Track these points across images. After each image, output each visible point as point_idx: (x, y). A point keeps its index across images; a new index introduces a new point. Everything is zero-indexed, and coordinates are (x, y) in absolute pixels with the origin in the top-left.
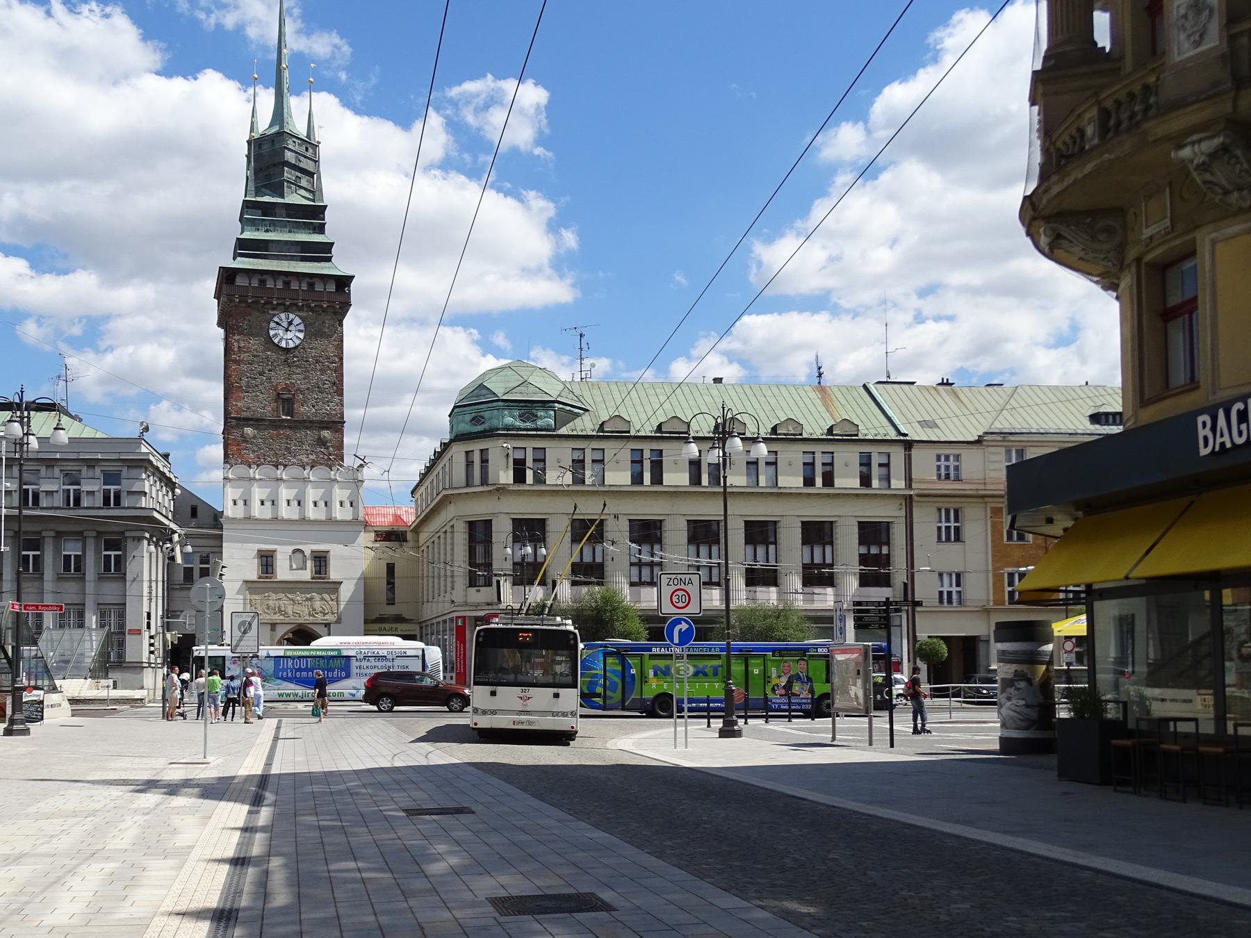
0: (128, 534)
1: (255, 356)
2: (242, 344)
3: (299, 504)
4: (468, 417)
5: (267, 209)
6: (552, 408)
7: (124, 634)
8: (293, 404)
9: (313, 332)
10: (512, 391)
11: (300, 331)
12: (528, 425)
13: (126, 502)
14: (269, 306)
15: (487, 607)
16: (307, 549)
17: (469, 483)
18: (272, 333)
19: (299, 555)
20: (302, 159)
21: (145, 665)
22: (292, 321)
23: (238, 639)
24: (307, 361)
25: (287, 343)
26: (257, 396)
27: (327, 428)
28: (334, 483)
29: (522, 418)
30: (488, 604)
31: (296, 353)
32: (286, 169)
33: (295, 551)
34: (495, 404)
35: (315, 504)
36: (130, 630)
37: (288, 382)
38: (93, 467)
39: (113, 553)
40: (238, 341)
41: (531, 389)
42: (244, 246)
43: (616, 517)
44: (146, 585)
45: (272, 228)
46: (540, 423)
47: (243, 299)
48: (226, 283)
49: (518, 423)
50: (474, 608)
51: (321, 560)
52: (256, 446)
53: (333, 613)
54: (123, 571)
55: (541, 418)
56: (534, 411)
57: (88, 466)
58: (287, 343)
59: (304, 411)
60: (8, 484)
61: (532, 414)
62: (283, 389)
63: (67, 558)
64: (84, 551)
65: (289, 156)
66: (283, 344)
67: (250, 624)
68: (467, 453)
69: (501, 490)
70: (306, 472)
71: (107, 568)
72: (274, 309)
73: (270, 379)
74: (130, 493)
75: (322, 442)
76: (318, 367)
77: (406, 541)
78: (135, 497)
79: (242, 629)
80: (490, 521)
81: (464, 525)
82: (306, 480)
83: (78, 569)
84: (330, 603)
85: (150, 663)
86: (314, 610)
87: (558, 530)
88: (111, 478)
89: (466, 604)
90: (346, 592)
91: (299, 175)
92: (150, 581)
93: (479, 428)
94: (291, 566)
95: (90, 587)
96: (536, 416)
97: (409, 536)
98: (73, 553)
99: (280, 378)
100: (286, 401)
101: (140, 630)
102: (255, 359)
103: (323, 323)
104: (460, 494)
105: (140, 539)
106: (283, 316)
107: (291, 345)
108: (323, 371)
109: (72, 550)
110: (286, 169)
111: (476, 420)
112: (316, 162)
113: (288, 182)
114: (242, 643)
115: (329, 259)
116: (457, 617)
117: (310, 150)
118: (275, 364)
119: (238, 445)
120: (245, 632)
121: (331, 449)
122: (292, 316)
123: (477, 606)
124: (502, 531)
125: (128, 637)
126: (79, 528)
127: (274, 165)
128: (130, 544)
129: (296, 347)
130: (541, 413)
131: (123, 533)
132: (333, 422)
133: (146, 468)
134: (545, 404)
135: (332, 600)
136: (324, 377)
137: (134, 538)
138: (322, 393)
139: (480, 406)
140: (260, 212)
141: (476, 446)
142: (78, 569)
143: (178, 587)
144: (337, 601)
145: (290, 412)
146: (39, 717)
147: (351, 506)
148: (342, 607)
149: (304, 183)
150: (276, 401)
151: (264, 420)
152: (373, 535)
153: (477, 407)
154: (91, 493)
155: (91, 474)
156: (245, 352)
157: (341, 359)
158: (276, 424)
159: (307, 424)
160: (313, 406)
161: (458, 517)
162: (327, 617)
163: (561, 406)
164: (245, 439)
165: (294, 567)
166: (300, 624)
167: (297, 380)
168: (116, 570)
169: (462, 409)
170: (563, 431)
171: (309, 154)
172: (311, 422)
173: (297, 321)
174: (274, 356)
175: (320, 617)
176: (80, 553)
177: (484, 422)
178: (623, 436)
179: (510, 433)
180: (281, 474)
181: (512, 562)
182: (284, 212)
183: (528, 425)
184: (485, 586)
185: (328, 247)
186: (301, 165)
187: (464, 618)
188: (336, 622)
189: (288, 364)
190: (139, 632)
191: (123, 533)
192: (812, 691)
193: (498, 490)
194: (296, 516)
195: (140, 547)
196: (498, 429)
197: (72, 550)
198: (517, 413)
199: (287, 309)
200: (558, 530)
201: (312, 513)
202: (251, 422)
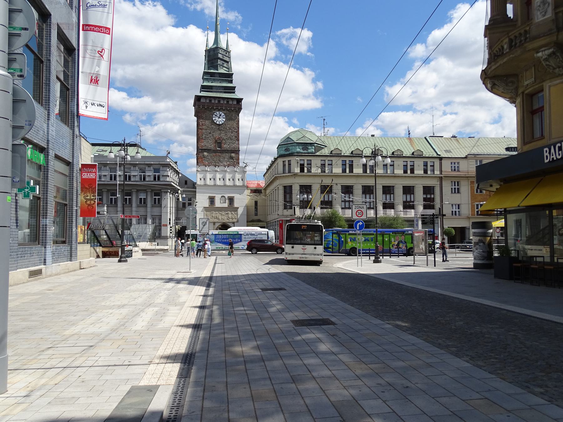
3: (223, 180)
4: (284, 149)
5: (212, 75)
7: (161, 226)
8: (221, 144)
9: (228, 119)
11: (224, 118)
12: (305, 151)
13: (161, 179)
18: (214, 119)
19: (223, 198)
20: (224, 57)
21: (168, 237)
25: (219, 122)
27: (233, 153)
29: (303, 149)
30: (291, 216)
33: (222, 197)
35: (229, 180)
37: (219, 136)
38: (150, 166)
39: (157, 197)
40: (202, 122)
41: (306, 139)
42: (204, 88)
43: (337, 184)
44: (169, 209)
45: (214, 81)
46: (309, 151)
49: (302, 151)
51: (231, 200)
53: (236, 219)
55: (310, 149)
58: (219, 122)
59: (225, 146)
60: (120, 173)
61: (307, 148)
62: (218, 139)
63: (141, 199)
65: (220, 56)
66: (218, 123)
67: (206, 223)
68: (283, 161)
69: (295, 175)
71: (155, 203)
72: (214, 110)
74: (163, 176)
75: (232, 158)
76: (230, 131)
79: (203, 224)
82: (226, 171)
83: (144, 203)
85: (170, 237)
86: (229, 217)
87: (316, 189)
88: (157, 170)
89: (283, 215)
90: (240, 211)
91: (224, 62)
92: (170, 207)
93: (288, 153)
94: (221, 202)
95: (149, 209)
96: (308, 148)
97: (263, 191)
99: (217, 135)
100: (219, 143)
102: (208, 128)
103: (232, 115)
105: (167, 192)
106: (218, 113)
107: (221, 123)
108: (232, 132)
109: (143, 196)
111: (287, 150)
113: (220, 65)
114: (203, 229)
117: (227, 54)
120: (204, 226)
122: (221, 113)
123: (287, 216)
124: (296, 189)
128: (163, 194)
129: (222, 124)
130: (310, 147)
132: (236, 150)
133: (169, 167)
134: (311, 144)
135: (235, 214)
136: (232, 135)
137: (164, 192)
140: (209, 75)
141: (287, 159)
142: (144, 203)
144: (237, 214)
145: (220, 147)
148: (239, 216)
149: (225, 65)
152: (250, 191)
154: (149, 176)
157: (239, 128)
158: (215, 151)
162: (233, 220)
163: (317, 145)
164: (204, 157)
165: (222, 202)
166: (224, 223)
167: (223, 135)
168: (158, 203)
169: (282, 146)
170: (318, 154)
172: (228, 150)
173: (223, 114)
175: (231, 220)
176: (145, 197)
178: (339, 155)
179: (299, 154)
182: (218, 76)
183: (305, 151)
186: (224, 59)
187: (282, 220)
188: (236, 222)
190: (166, 225)
192: (406, 246)
193: (294, 175)
194: (222, 184)
196: (295, 153)
197: (143, 196)
198: (301, 147)
199: (219, 110)
200: (316, 189)
201: (228, 183)
202: (206, 151)
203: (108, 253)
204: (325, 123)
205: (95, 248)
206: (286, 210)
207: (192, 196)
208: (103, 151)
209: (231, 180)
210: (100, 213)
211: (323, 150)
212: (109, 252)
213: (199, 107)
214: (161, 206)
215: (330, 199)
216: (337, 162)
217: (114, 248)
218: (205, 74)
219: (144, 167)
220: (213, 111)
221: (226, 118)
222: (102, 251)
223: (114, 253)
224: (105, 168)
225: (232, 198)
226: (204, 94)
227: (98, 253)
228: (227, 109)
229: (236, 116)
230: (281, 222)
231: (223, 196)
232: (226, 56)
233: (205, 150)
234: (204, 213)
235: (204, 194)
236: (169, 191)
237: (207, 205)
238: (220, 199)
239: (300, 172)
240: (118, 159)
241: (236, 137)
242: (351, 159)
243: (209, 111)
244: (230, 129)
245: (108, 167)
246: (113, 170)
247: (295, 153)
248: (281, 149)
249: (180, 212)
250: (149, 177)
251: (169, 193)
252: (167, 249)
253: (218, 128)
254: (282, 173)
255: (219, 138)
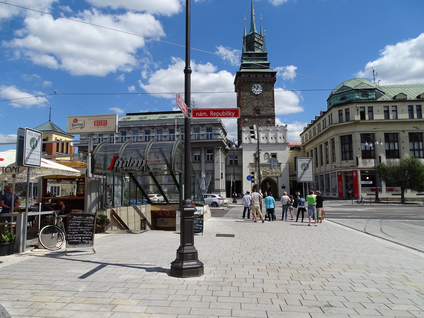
0: (214, 148)
1: (247, 97)
2: (244, 94)
3: (266, 138)
4: (339, 98)
5: (250, 55)
6: (374, 91)
7: (214, 180)
8: (259, 111)
9: (265, 90)
10: (358, 86)
11: (261, 89)
12: (365, 98)
13: (214, 137)
14: (252, 82)
15: (352, 168)
16: (270, 153)
17: (341, 121)
18: (253, 90)
19: (267, 155)
20: (259, 40)
21: (221, 190)
22: (259, 86)
23: (301, 173)
24: (263, 98)
25: (257, 93)
26: (249, 109)
27: (270, 118)
28: (277, 131)
29: (362, 96)
30: (352, 166)
31: (260, 96)
32: (255, 43)
33: (266, 153)
34: (351, 91)
35: (272, 138)
36: (216, 179)
37: (258, 105)
38: (203, 126)
39: (210, 154)
40: (243, 93)
41: (365, 85)
42: (244, 66)
43: (404, 131)
44: (220, 163)
45: (251, 60)
46: (370, 97)
47: (244, 81)
48: (239, 76)
49: (361, 98)
50: (346, 168)
51: (274, 156)
52: (249, 124)
53: (279, 173)
54: (213, 160)
55: (370, 95)
56: (367, 93)
57: (202, 126)
58: (257, 93)
59: (263, 113)
60: (177, 133)
62: (256, 107)
63: (196, 156)
64: (201, 154)
65: (256, 39)
66: (256, 93)
67: (308, 165)
68: (339, 111)
69: (356, 123)
70: (268, 128)
71: (208, 159)
72: (253, 83)
73: (252, 104)
74: (215, 134)
75: (268, 122)
76: (267, 100)
77: (301, 150)
78: (216, 136)
79: (304, 168)
80: (351, 135)
81: (339, 137)
82: (268, 131)
83: (199, 159)
84: (278, 170)
85: (222, 190)
86: (273, 172)
87: (380, 136)
88: (209, 130)
89: (342, 167)
90: (283, 166)
91: (259, 45)
92: (221, 163)
93: (344, 101)
94: (265, 158)
95: (203, 164)
97: (302, 148)
98: (197, 154)
99: (255, 103)
100: (257, 110)
101: (219, 179)
102: (248, 98)
103: (268, 86)
104: (337, 126)
105: (218, 149)
106: (256, 85)
107: (258, 93)
108: (268, 101)
109: (197, 154)
110: (255, 43)
112: (263, 41)
113: (256, 47)
114: (304, 176)
115: (269, 68)
116: (338, 172)
117: (262, 38)
118: (254, 99)
119: (243, 124)
120: (305, 170)
121: (271, 124)
122: (258, 85)
123: (347, 168)
124: (356, 138)
125: (215, 181)
126: (199, 146)
127: (251, 43)
128: (215, 151)
129: (260, 94)
131: (213, 147)
132: (272, 116)
133: (220, 126)
134: (372, 90)
135: (278, 169)
136: (269, 103)
137: (216, 149)
138: (268, 107)
139: (344, 93)
140: (248, 56)
141: (343, 108)
142: (199, 159)
143: (228, 166)
144: (280, 169)
145: (259, 113)
146: (200, 228)
147: (283, 138)
148: (282, 170)
149: (260, 47)
150: (254, 110)
151: (251, 116)
152: (290, 148)
153: (343, 94)
154: (203, 135)
155: (203, 129)
156: (245, 96)
157: (274, 97)
158: (255, 117)
159: (264, 117)
160: (266, 111)
161: (336, 135)
162: (277, 175)
163: (377, 91)
164: (245, 122)
165: (266, 158)
166: (268, 177)
167: (261, 104)
168: (211, 160)
169: (336, 95)
170: (379, 100)
171: (262, 39)
172: (265, 116)
173: (260, 86)
174: (253, 97)
175: (274, 175)
176: (199, 154)
177: (346, 99)
178: (404, 101)
179: (358, 101)
180: (261, 129)
181: (361, 150)
182: (255, 55)
183: (365, 98)
184: (349, 160)
185: (268, 64)
186: (259, 42)
187: (341, 172)
188: (280, 176)
189: (258, 99)
190: (219, 180)
191: (213, 147)
192: (166, 193)
193: (355, 123)
194: (266, 142)
195: (219, 152)
196: (354, 100)
197: (197, 154)
198: (360, 94)
199: (257, 83)
200: (380, 136)
201: (271, 141)
202: (247, 117)
203: (161, 214)
204: (375, 74)
205: (138, 207)
206: (345, 161)
207: (238, 154)
208: (164, 117)
209: (274, 138)
210: (162, 169)
211: (382, 97)
212: (163, 212)
213: (240, 81)
214: (213, 162)
215: (396, 148)
216: (403, 109)
217: (168, 206)
218: (244, 55)
219: (198, 127)
220: (252, 84)
221: (263, 89)
222: (151, 211)
223: (169, 214)
224: (165, 129)
225: (275, 154)
226: (244, 70)
227: (144, 215)
228: (263, 82)
229: (271, 87)
230: (339, 174)
231: (267, 153)
232: (260, 40)
233: (245, 116)
234: (250, 168)
235: (250, 152)
236: (221, 148)
237: (252, 161)
238: (264, 156)
239: (361, 119)
240: (176, 121)
241: (272, 104)
242: (418, 104)
243: (248, 84)
244: (266, 98)
245: (167, 129)
246: (172, 131)
247: (354, 100)
248: (335, 98)
249: (228, 168)
250: (203, 136)
251: (220, 150)
252: (226, 203)
253: (256, 97)
254: (338, 122)
255: (257, 106)
